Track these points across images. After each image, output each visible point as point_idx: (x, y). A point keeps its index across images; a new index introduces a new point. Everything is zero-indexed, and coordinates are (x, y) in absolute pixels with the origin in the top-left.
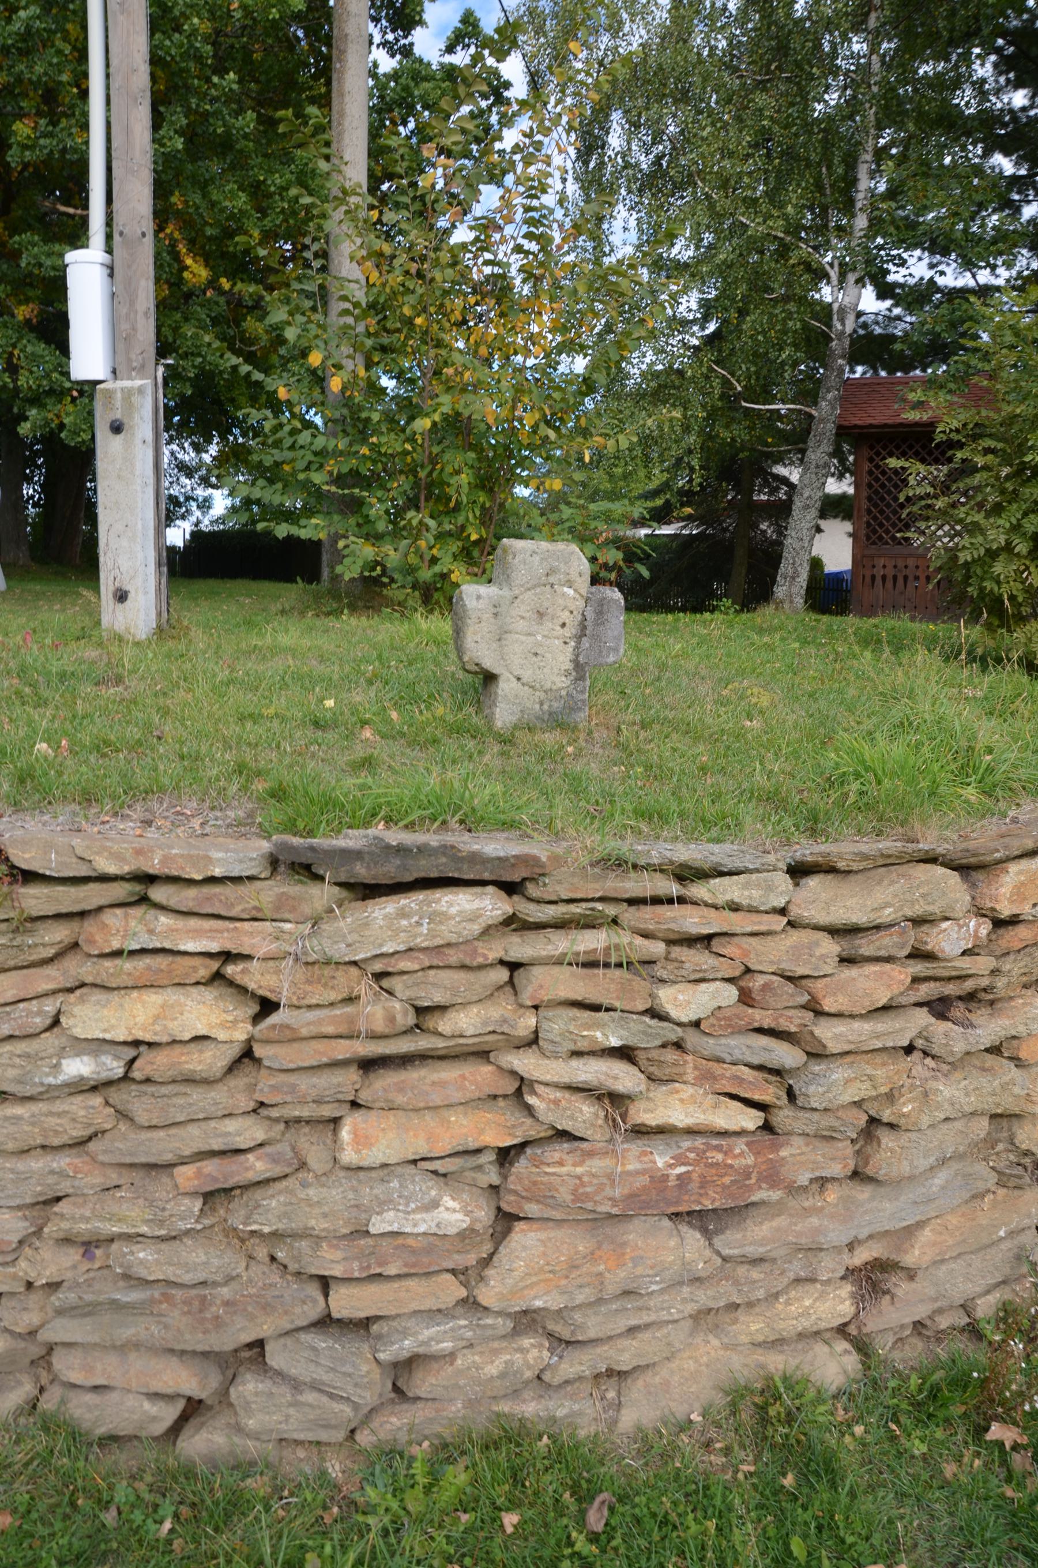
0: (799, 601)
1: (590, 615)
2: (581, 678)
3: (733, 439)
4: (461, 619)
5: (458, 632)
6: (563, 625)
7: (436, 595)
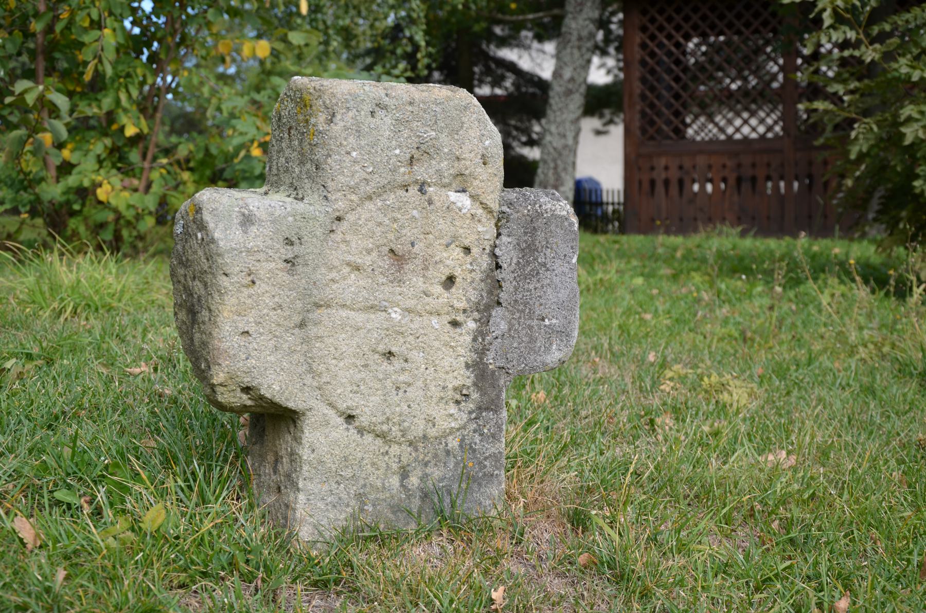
1: (508, 255)
2: (490, 405)
4: (200, 276)
5: (192, 312)
6: (450, 281)
7: (73, 223)
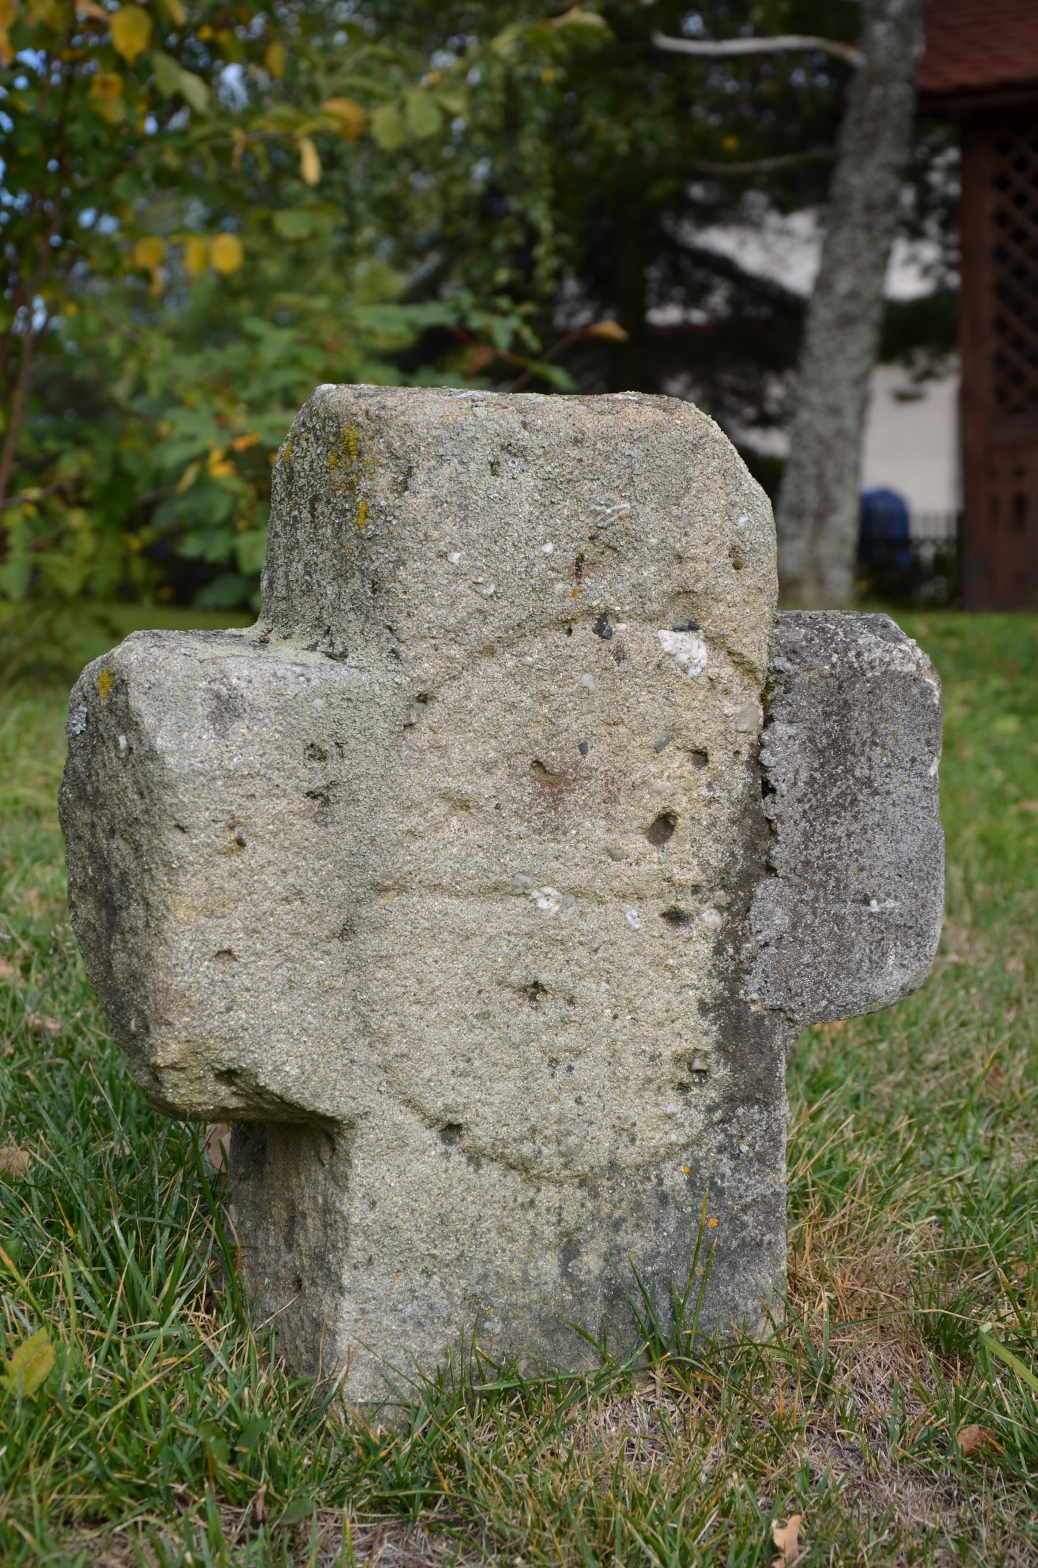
0: (841, 579)
1: (789, 762)
3: (635, 146)
6: (663, 826)
